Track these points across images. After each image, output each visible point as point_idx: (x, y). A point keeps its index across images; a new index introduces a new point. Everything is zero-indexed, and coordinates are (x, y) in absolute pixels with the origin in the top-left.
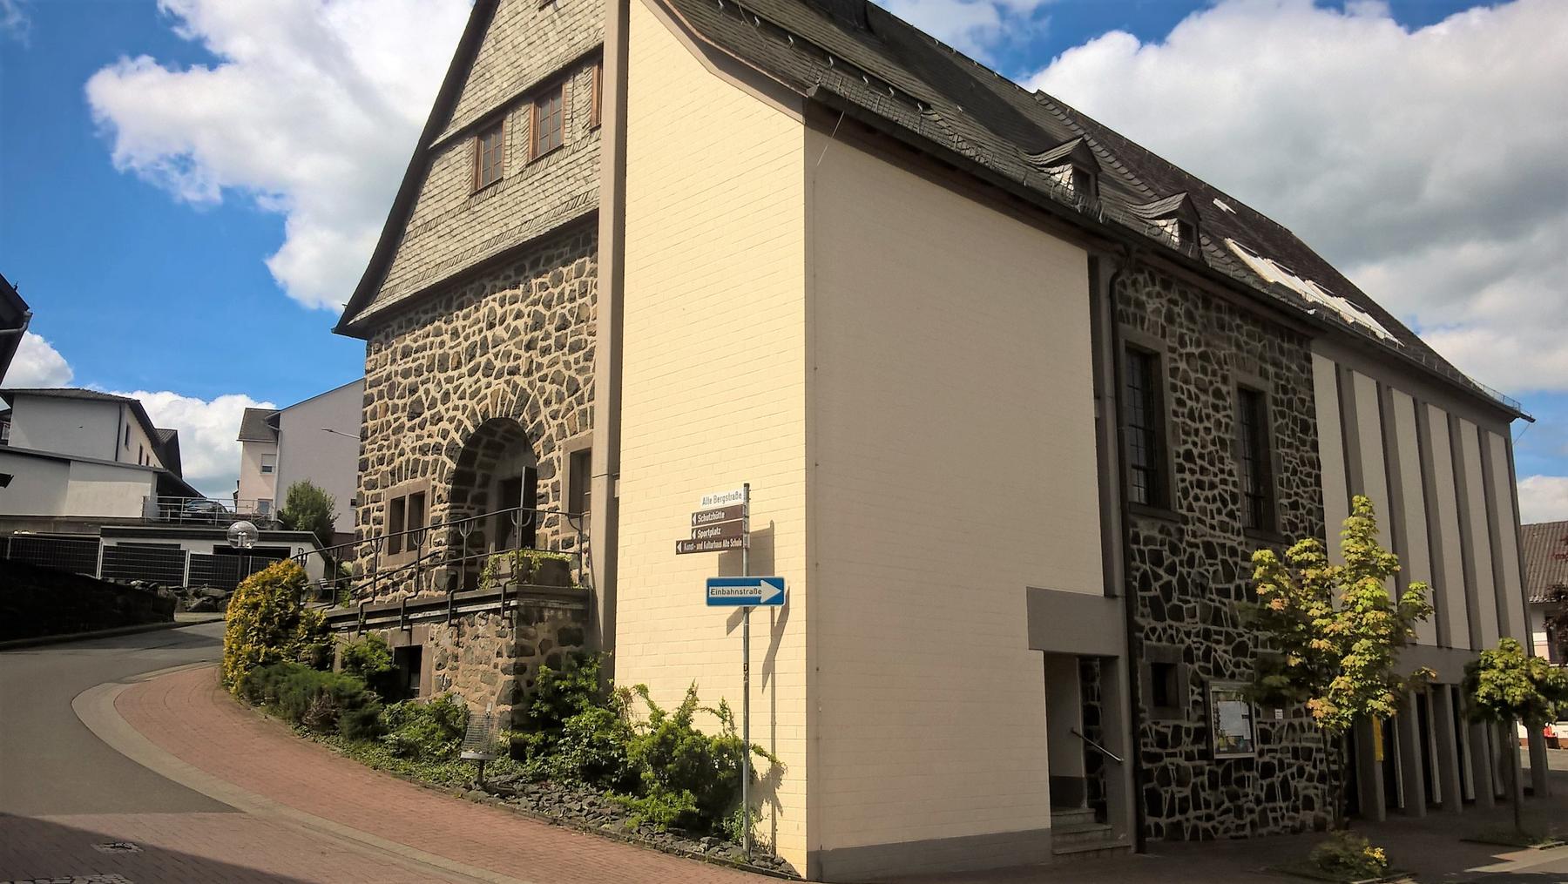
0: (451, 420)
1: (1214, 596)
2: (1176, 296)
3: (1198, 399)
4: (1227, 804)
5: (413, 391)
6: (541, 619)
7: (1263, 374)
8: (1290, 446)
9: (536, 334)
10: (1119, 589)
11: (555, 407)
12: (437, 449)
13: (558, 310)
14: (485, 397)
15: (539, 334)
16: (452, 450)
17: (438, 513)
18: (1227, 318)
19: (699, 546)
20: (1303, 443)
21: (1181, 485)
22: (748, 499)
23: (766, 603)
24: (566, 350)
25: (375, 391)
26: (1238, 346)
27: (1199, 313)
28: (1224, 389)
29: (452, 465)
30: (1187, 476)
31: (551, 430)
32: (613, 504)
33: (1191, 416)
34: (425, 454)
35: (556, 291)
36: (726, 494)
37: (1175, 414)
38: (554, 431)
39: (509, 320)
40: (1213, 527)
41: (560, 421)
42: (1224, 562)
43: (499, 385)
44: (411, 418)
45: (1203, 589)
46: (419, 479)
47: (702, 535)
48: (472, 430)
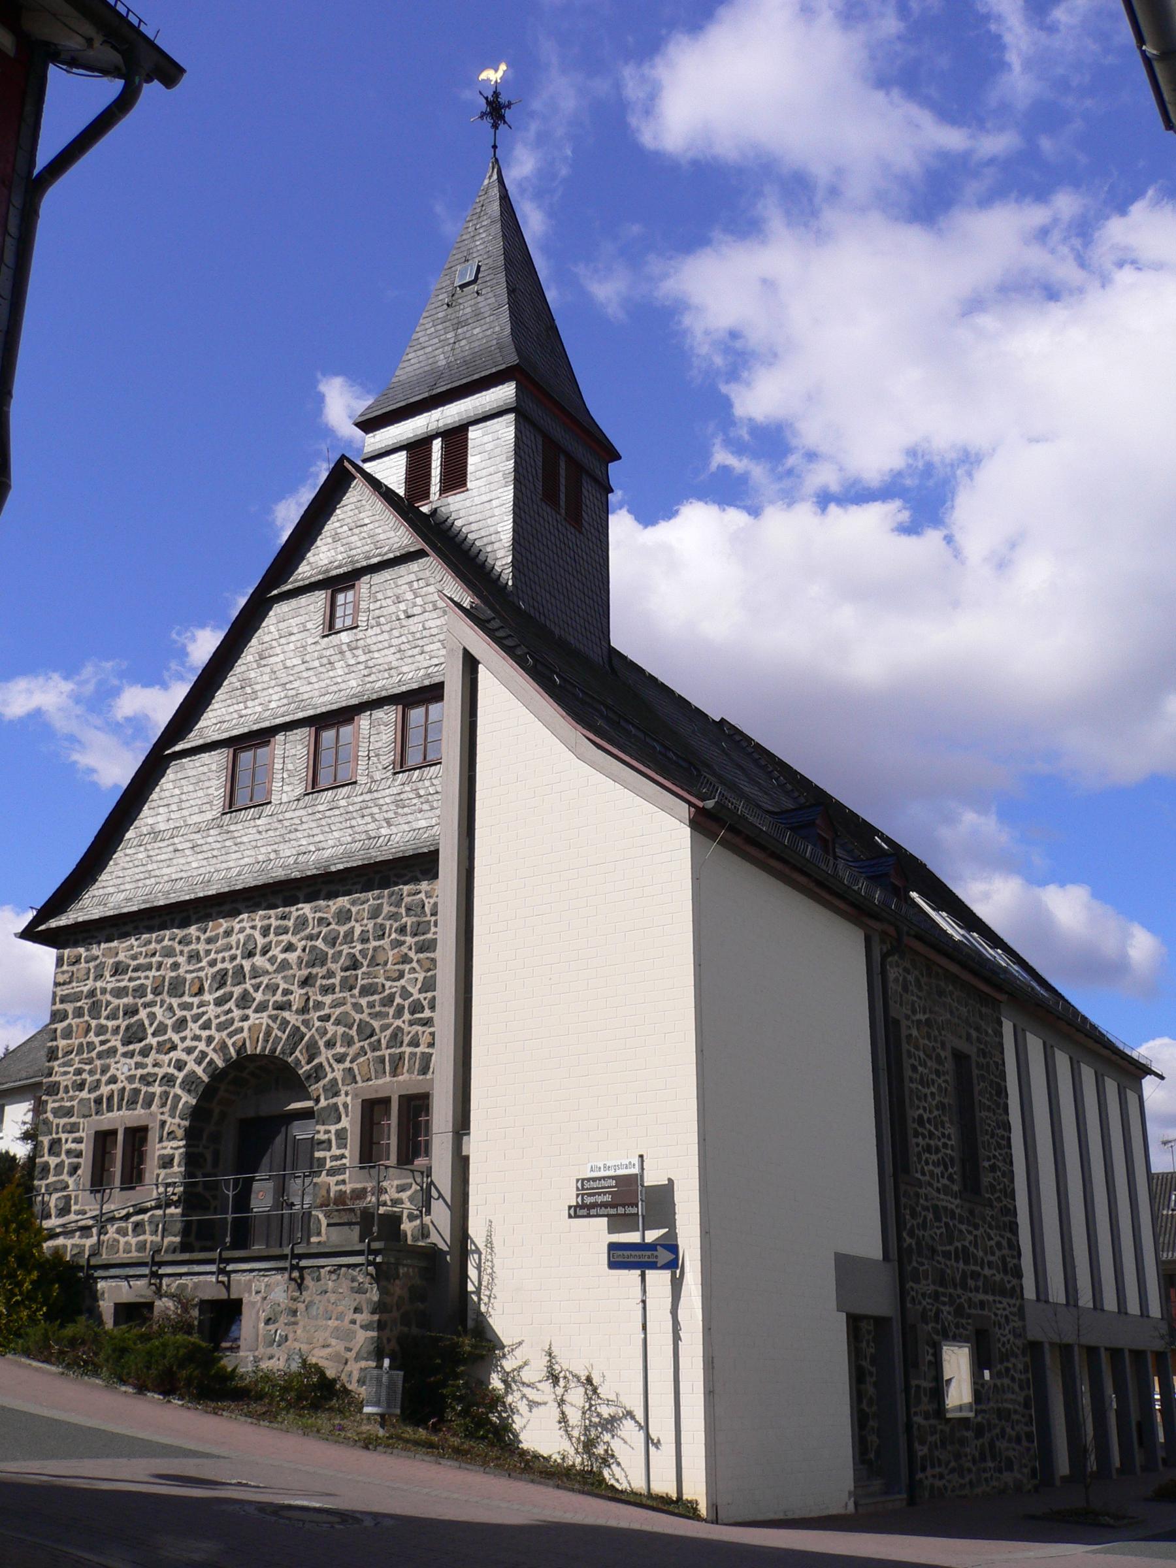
0: (189, 1051)
1: (940, 1259)
2: (908, 966)
3: (925, 1066)
4: (953, 1464)
5: (131, 1011)
6: (398, 1277)
7: (969, 1038)
8: (989, 1109)
9: (314, 971)
10: (894, 1254)
11: (339, 1049)
12: (169, 1080)
13: (346, 949)
14: (241, 1030)
15: (319, 971)
16: (190, 1083)
17: (168, 1151)
18: (942, 984)
19: (593, 1212)
20: (998, 1105)
21: (916, 1150)
22: (643, 1169)
23: (663, 1267)
24: (356, 991)
25: (69, 1007)
26: (952, 1013)
27: (923, 980)
28: (943, 1054)
29: (188, 1099)
30: (920, 1140)
31: (336, 1073)
32: (461, 1165)
33: (922, 1082)
34: (149, 1084)
35: (343, 929)
36: (621, 1163)
37: (911, 1080)
38: (338, 1075)
39: (275, 951)
40: (938, 1190)
41: (347, 1064)
42: (947, 1224)
43: (264, 1019)
44: (127, 1042)
45: (933, 1251)
46: (140, 1111)
47: (588, 1200)
48: (220, 1064)
